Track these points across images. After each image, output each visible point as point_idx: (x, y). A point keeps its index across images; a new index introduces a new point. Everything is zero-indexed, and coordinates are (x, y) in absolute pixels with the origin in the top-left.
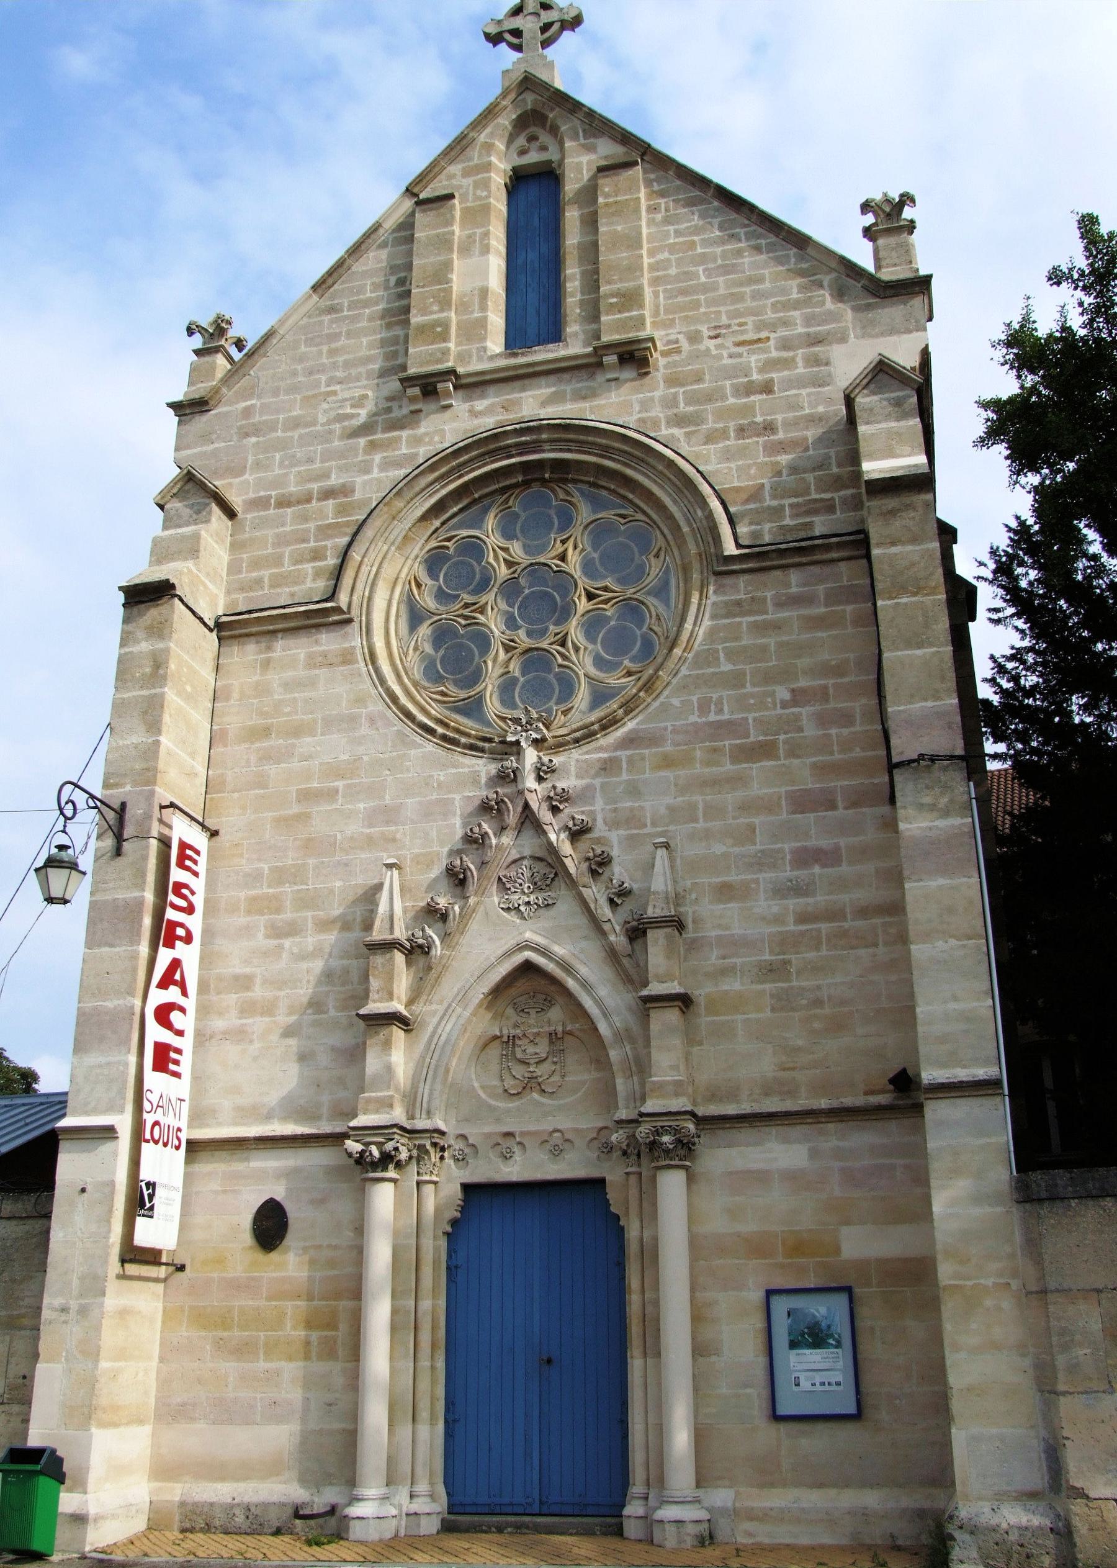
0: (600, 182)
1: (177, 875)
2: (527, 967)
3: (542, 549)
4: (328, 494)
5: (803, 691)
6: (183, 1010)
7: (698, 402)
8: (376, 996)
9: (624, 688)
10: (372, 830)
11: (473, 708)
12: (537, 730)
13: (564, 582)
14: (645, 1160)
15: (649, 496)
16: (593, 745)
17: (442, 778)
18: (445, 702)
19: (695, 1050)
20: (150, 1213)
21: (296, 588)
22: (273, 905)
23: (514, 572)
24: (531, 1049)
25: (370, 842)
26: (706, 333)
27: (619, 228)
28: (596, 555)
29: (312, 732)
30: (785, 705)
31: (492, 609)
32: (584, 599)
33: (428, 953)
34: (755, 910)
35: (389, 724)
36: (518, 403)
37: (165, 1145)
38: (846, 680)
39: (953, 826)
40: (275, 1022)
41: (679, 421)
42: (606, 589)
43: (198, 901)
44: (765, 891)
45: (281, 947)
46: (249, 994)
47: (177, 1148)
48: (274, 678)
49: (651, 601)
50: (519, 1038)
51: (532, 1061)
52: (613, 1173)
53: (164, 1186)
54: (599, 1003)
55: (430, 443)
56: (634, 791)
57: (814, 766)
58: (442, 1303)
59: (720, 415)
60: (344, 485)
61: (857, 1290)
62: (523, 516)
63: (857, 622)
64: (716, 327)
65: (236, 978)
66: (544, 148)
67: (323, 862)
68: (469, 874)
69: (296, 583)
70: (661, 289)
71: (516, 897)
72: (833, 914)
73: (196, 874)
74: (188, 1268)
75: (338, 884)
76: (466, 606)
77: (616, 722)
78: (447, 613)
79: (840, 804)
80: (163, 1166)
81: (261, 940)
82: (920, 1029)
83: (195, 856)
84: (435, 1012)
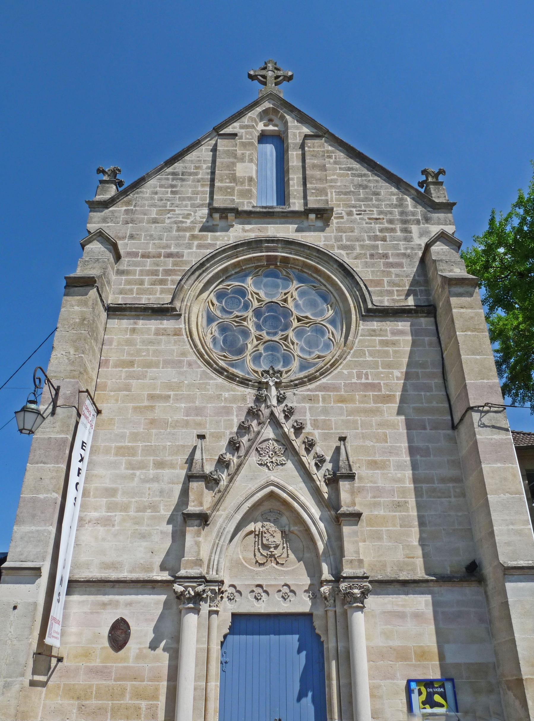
0: (306, 141)
3: (273, 295)
4: (170, 255)
7: (352, 241)
8: (193, 504)
9: (317, 364)
10: (188, 418)
12: (277, 378)
17: (227, 396)
18: (225, 360)
21: (151, 296)
22: (131, 451)
23: (261, 304)
24: (271, 539)
25: (186, 424)
26: (355, 212)
27: (316, 162)
29: (157, 365)
31: (250, 320)
32: (296, 320)
33: (218, 484)
34: (389, 475)
35: (199, 367)
36: (267, 229)
40: (128, 515)
42: (307, 317)
44: (394, 466)
45: (134, 475)
46: (114, 499)
48: (137, 338)
50: (265, 533)
51: (272, 546)
55: (222, 240)
56: (325, 411)
59: (362, 247)
60: (178, 252)
64: (359, 211)
65: (107, 490)
67: (160, 432)
68: (242, 444)
70: (333, 190)
74: (65, 660)
75: (169, 444)
76: (237, 317)
78: (227, 319)
79: (428, 427)
81: (123, 470)
84: (221, 515)
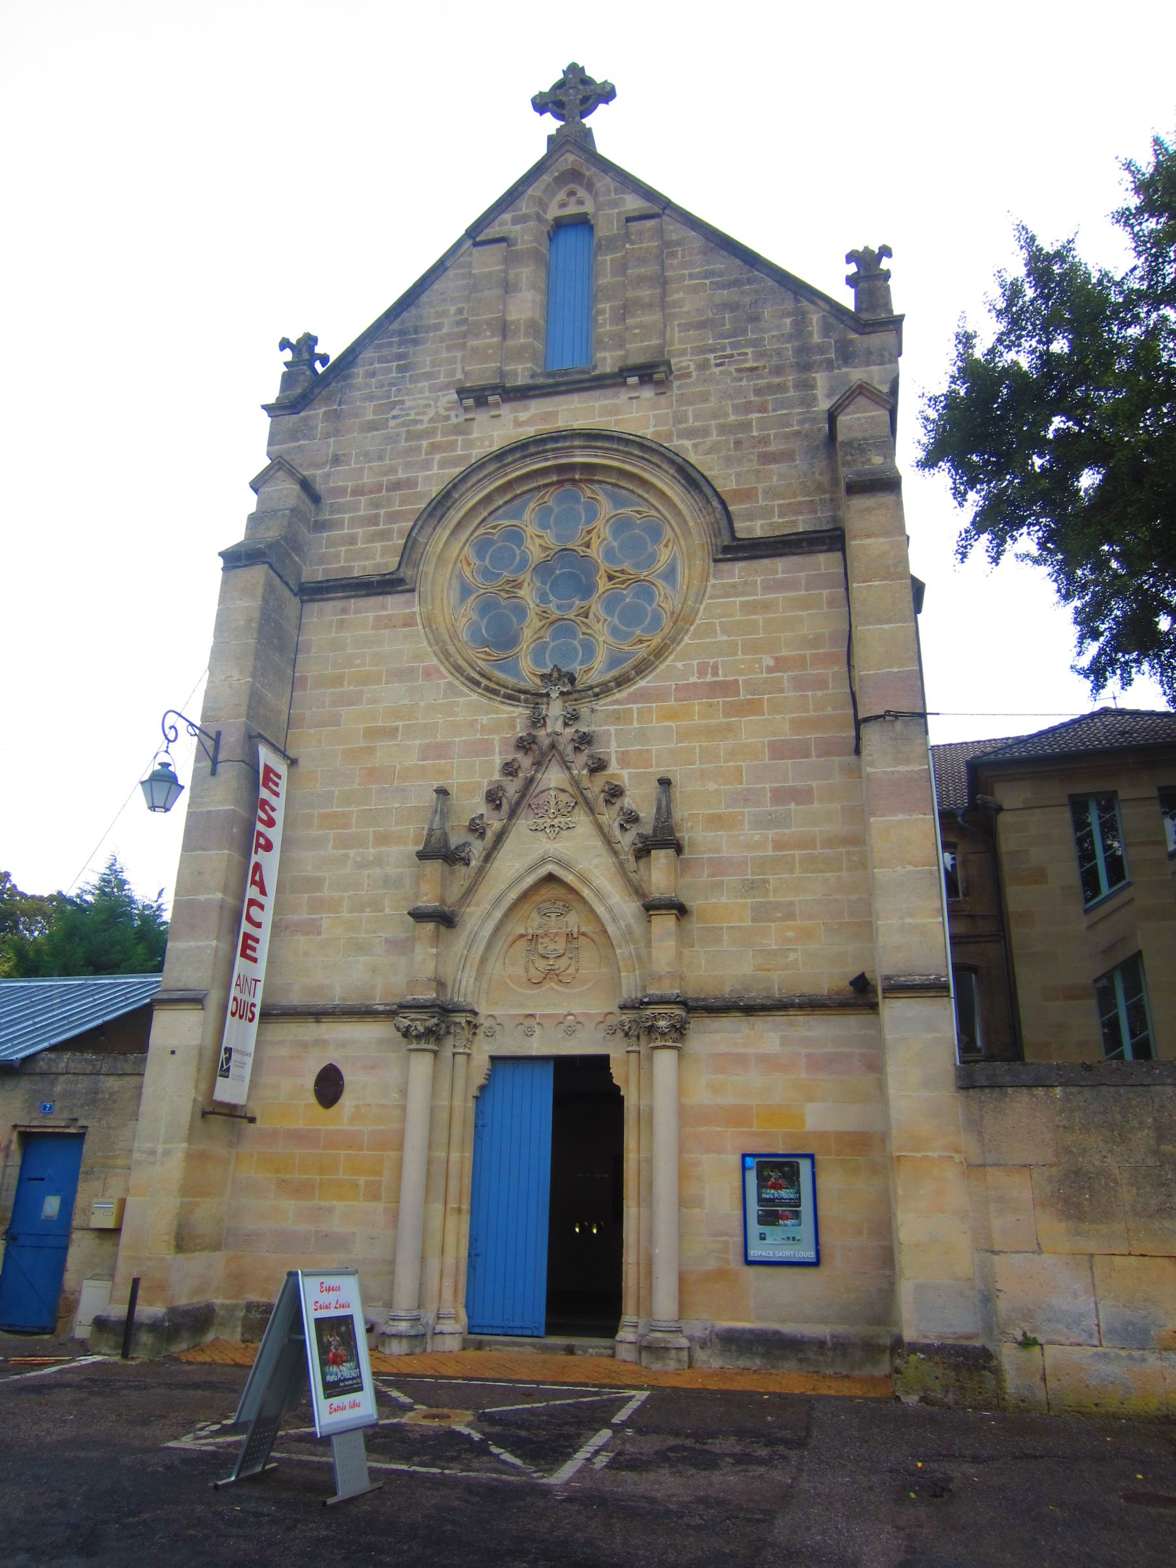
1: (264, 794)
2: (551, 878)
5: (786, 659)
6: (262, 907)
11: (511, 667)
13: (587, 566)
14: (643, 1039)
15: (662, 494)
16: (608, 699)
19: (686, 951)
20: (225, 1073)
21: (367, 563)
24: (552, 947)
26: (713, 362)
28: (615, 544)
30: (770, 670)
35: (443, 677)
36: (554, 415)
37: (241, 1017)
38: (822, 651)
39: (912, 771)
41: (689, 434)
42: (623, 572)
43: (278, 816)
47: (251, 1020)
49: (660, 583)
52: (616, 1051)
53: (238, 1051)
54: (610, 910)
57: (792, 721)
58: (469, 1154)
60: (408, 479)
61: (817, 1157)
62: (556, 510)
63: (831, 603)
66: (581, 202)
69: (367, 559)
71: (542, 820)
72: (805, 843)
73: (277, 794)
76: (508, 582)
77: (629, 680)
80: (243, 1035)
82: (881, 940)
83: (276, 779)
